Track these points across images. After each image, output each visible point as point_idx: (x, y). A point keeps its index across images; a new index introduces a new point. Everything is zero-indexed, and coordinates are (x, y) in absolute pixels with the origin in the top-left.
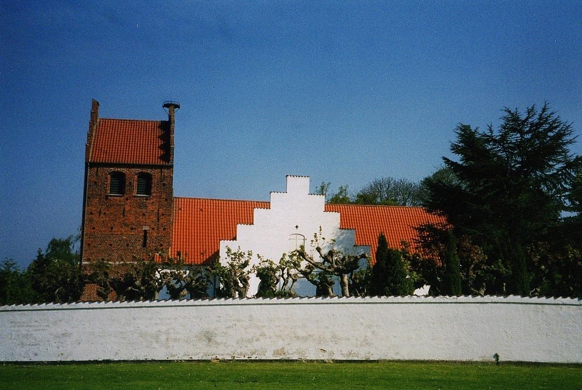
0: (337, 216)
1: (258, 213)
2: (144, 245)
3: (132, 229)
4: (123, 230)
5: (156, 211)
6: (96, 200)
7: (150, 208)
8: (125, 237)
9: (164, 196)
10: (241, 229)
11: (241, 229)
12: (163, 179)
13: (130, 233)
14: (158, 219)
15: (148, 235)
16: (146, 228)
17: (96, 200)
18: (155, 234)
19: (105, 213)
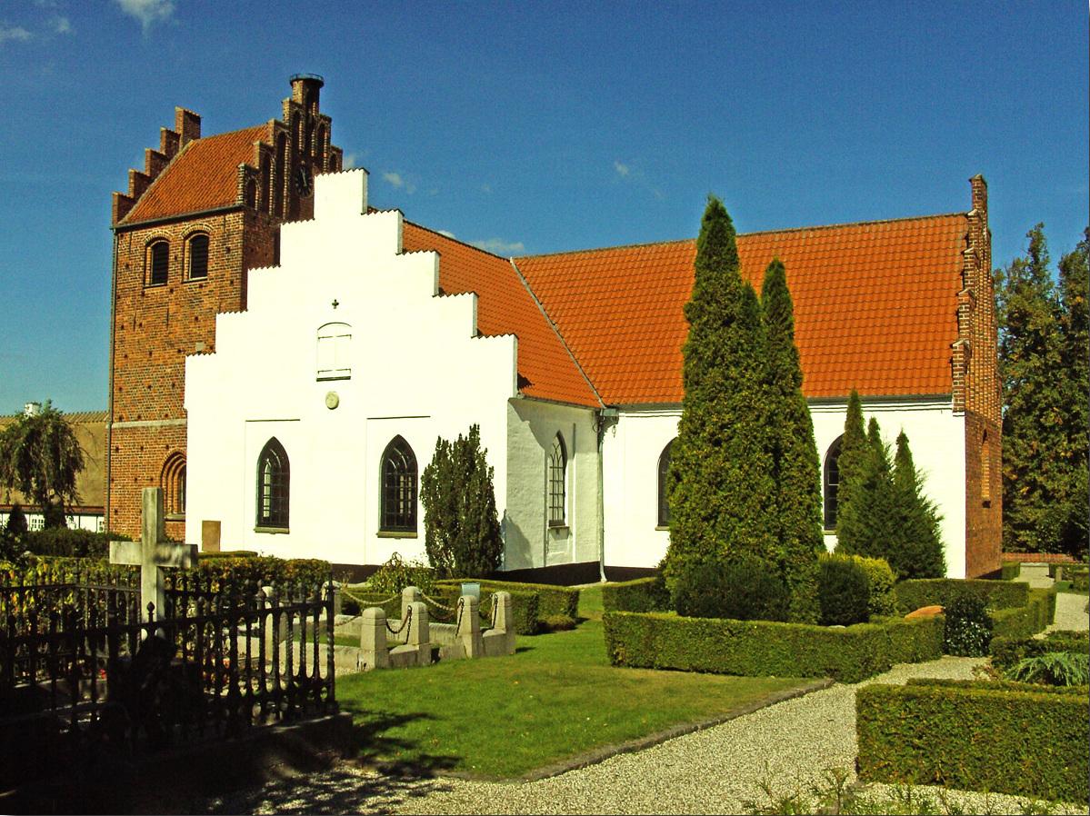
3: (179, 351)
19: (141, 325)
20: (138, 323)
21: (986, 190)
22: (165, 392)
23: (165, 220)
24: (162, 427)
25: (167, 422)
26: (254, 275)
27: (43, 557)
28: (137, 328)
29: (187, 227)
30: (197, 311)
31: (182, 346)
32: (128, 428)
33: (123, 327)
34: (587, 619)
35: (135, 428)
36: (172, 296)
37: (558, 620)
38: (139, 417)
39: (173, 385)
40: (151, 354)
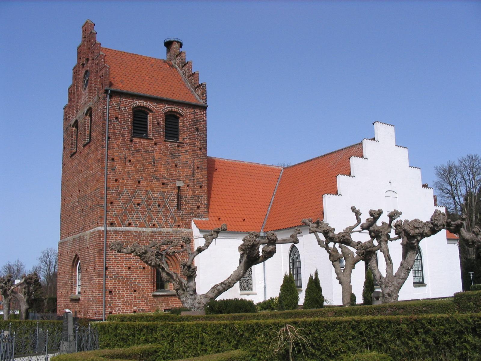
0: (195, 266)
1: (355, 162)
2: (179, 206)
3: (163, 184)
4: (154, 186)
5: (190, 162)
6: (119, 142)
7: (184, 157)
8: (156, 195)
9: (198, 143)
10: (342, 180)
11: (342, 180)
12: (196, 122)
13: (162, 190)
14: (193, 173)
15: (182, 193)
16: (180, 184)
17: (119, 142)
18: (191, 192)
19: (130, 161)
20: (128, 159)
21: (155, 59)
22: (153, 209)
23: (168, 104)
24: (152, 232)
25: (155, 229)
26: (355, 213)
27: (185, 306)
28: (127, 163)
29: (168, 108)
30: (176, 161)
31: (165, 181)
32: (122, 232)
33: (113, 159)
34: (317, 270)
35: (129, 232)
36: (157, 148)
37: (459, 223)
38: (130, 224)
39: (159, 205)
40: (139, 182)
